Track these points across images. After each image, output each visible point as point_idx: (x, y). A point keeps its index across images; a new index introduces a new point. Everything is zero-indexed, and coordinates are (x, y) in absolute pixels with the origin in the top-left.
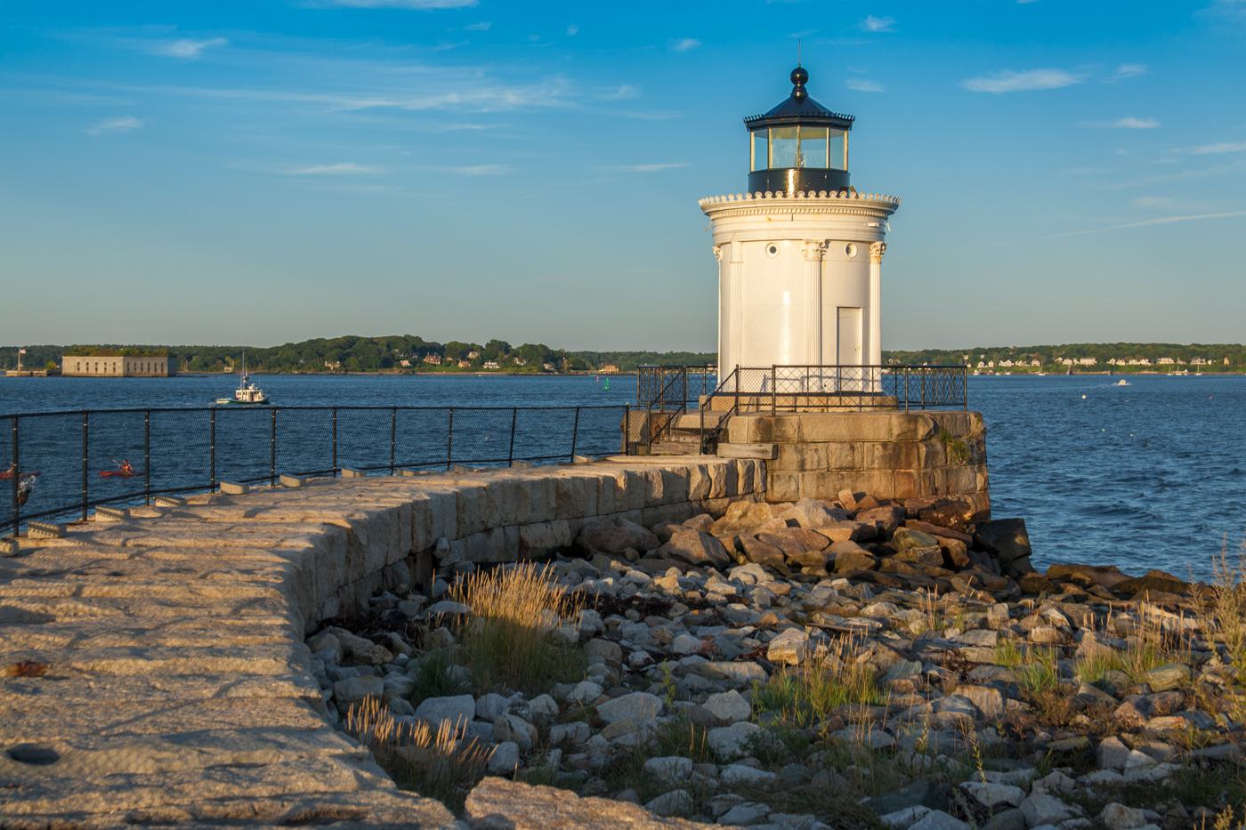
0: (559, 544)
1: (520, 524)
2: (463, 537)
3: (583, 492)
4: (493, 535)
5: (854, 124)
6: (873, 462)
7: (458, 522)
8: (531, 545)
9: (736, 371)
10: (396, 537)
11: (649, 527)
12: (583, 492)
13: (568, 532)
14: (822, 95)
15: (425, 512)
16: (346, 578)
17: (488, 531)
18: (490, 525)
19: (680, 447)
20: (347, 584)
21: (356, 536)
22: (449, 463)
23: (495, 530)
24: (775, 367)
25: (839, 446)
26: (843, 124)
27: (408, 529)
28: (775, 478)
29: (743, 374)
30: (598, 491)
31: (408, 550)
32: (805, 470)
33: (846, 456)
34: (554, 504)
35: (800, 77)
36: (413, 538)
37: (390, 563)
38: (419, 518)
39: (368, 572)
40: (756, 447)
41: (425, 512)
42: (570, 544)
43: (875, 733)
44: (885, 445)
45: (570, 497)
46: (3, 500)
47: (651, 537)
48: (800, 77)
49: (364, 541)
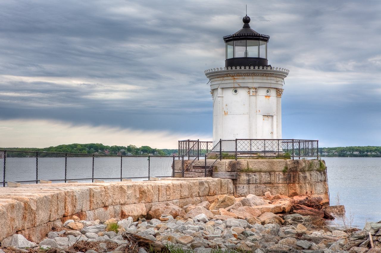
0: (140, 214)
1: (122, 204)
2: (93, 209)
3: (152, 191)
4: (108, 209)
5: (269, 40)
6: (279, 181)
7: (91, 202)
8: (127, 214)
9: (221, 142)
10: (56, 208)
11: (182, 207)
12: (152, 191)
13: (145, 209)
14: (255, 26)
15: (73, 197)
16: (23, 226)
17: (106, 207)
18: (107, 204)
19: (197, 174)
20: (24, 230)
21: (29, 205)
22: (93, 179)
23: (109, 207)
24: (237, 140)
25: (265, 173)
26: (265, 39)
27: (63, 204)
28: (237, 187)
29: (223, 143)
30: (159, 191)
31: (63, 214)
32: (250, 184)
33: (267, 178)
34: (138, 196)
35: (246, 21)
36: (65, 209)
37: (52, 220)
38: (69, 200)
39: (38, 224)
40: (229, 173)
41: (73, 197)
42: (146, 214)
43: (99, 188)
44: (284, 172)
45: (146, 193)
46: (168, 252)
47: (182, 211)
48: (246, 21)
49: (34, 208)
